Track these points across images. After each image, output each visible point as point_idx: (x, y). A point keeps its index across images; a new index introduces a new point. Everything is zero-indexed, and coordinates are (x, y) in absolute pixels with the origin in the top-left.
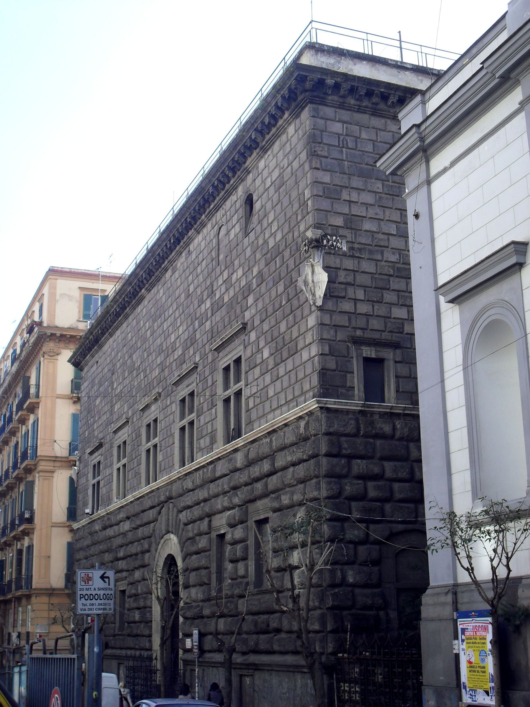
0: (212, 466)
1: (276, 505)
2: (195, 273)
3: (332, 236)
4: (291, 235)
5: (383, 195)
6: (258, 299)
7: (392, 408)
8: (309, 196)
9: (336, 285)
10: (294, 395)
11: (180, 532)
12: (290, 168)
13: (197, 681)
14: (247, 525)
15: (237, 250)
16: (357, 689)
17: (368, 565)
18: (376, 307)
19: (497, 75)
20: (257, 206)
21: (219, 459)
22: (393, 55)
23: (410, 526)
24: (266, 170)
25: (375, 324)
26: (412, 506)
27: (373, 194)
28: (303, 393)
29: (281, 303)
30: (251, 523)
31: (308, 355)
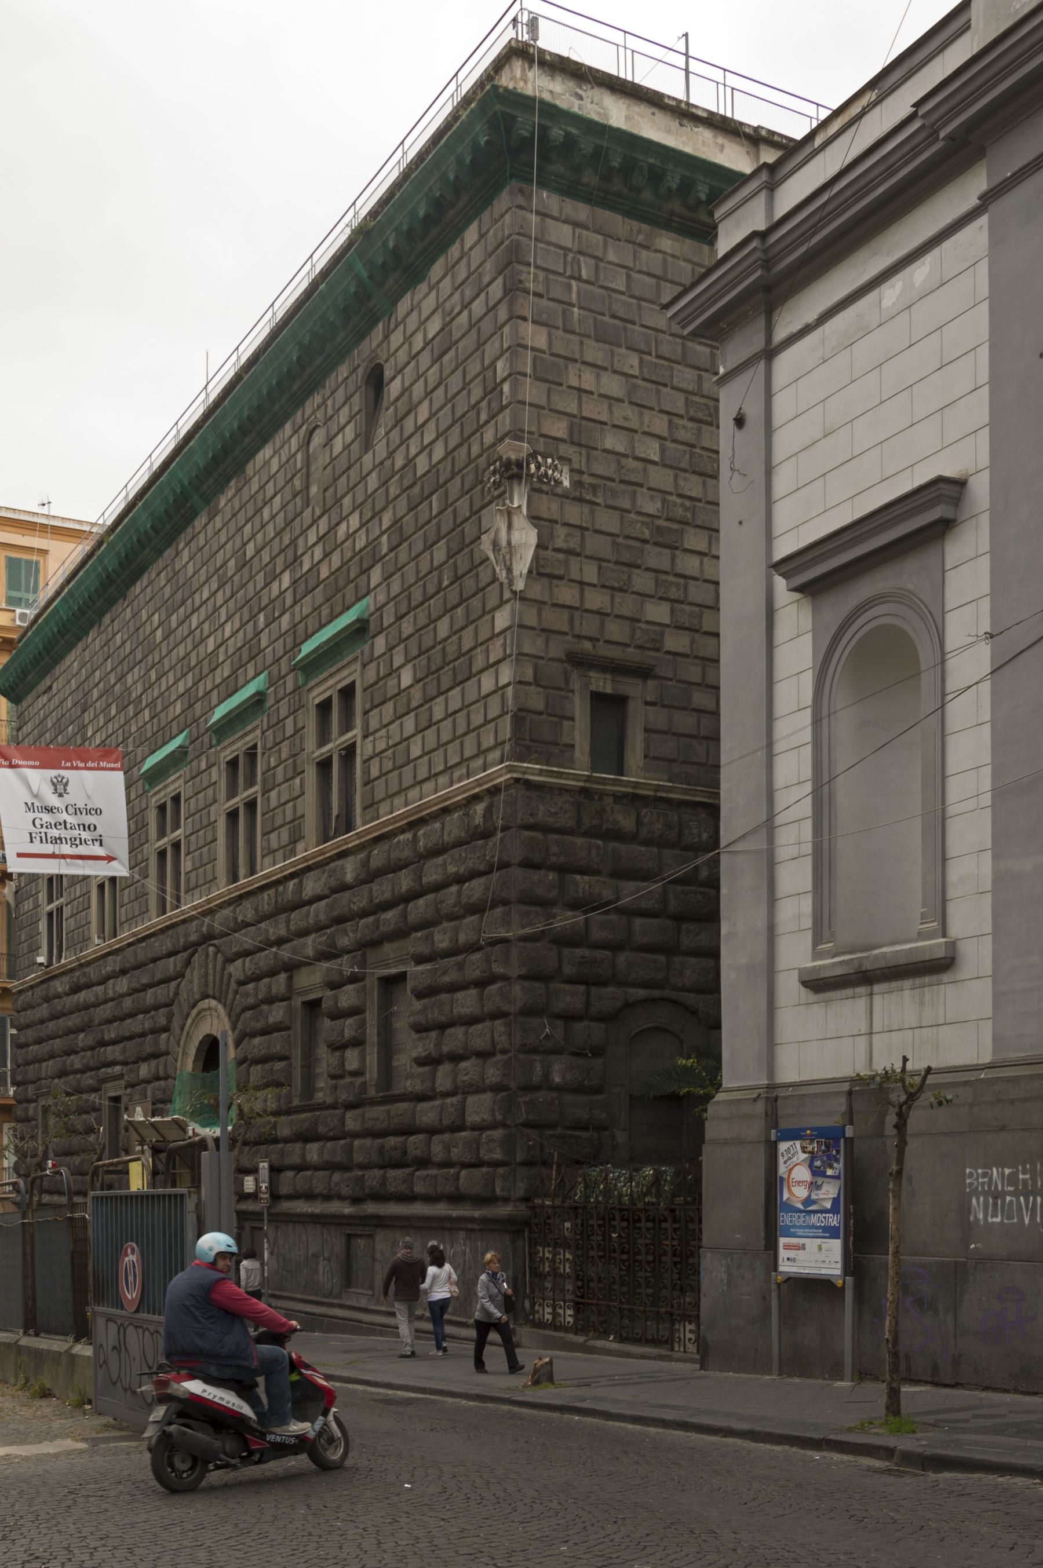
0: (296, 881)
1: (424, 949)
2: (257, 519)
3: (545, 457)
4: (463, 451)
5: (640, 382)
6: (392, 575)
7: (636, 785)
8: (505, 374)
9: (549, 553)
10: (462, 755)
11: (230, 996)
12: (465, 313)
13: (266, 1245)
14: (365, 986)
15: (348, 477)
16: (568, 1256)
17: (586, 1055)
18: (617, 600)
19: (942, 134)
20: (394, 388)
21: (309, 869)
22: (671, 86)
23: (656, 993)
24: (414, 315)
25: (615, 630)
26: (662, 958)
27: (623, 379)
28: (481, 752)
29: (440, 582)
30: (371, 983)
31: (494, 681)
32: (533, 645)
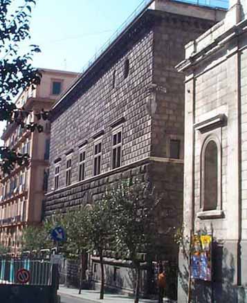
32: (156, 129)
